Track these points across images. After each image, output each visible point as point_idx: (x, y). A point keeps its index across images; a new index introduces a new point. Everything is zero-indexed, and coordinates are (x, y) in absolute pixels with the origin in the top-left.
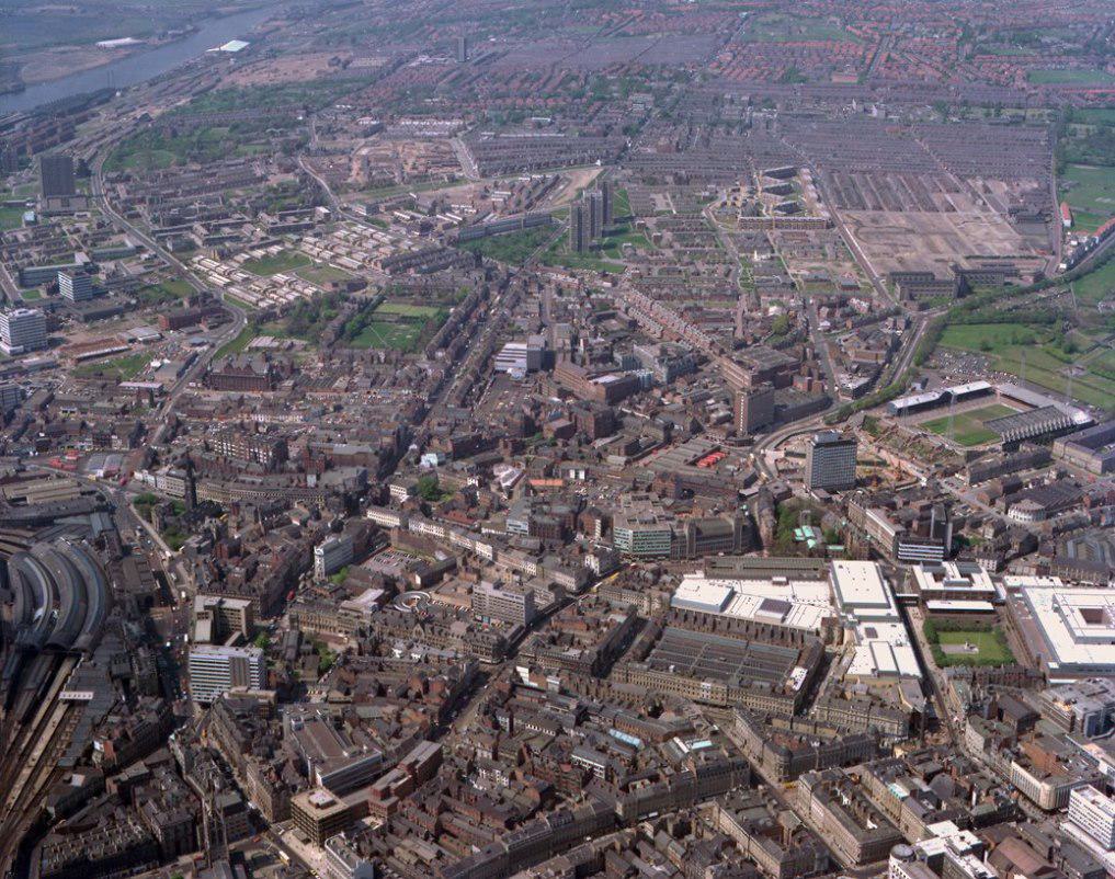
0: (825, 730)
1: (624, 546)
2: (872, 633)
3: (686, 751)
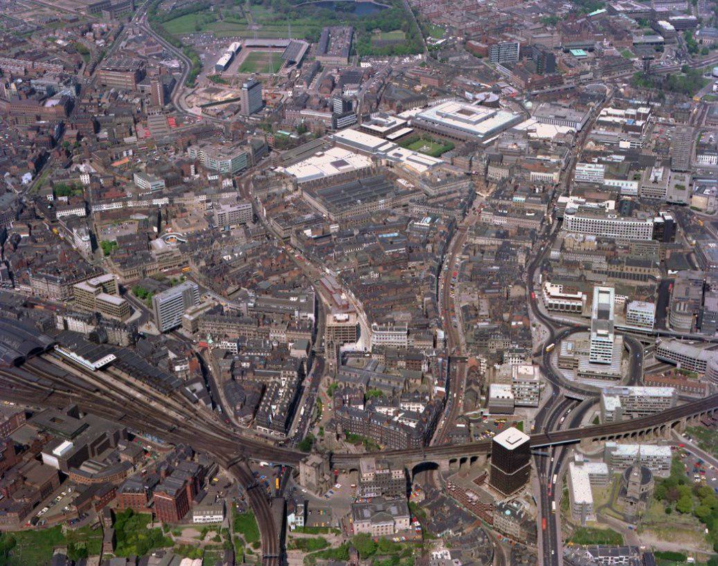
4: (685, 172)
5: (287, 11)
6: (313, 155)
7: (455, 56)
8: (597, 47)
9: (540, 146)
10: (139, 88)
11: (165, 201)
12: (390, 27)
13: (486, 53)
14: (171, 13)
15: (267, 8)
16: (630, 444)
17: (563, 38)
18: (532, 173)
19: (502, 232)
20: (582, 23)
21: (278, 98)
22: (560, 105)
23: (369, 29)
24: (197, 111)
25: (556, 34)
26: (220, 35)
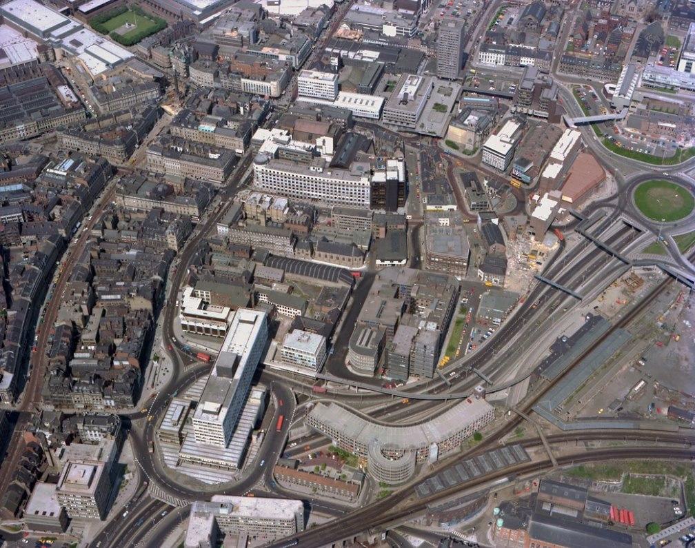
0: (121, 116)
2: (77, 43)
3: (65, 174)
4: (455, 80)
16: (486, 140)
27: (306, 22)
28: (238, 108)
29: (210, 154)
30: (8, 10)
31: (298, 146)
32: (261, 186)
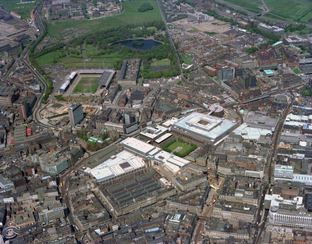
1: (54, 172)
3: (179, 222)
5: (105, 48)
6: (109, 158)
7: (198, 77)
8: (279, 68)
9: (250, 146)
10: (14, 106)
11: (10, 200)
12: (162, 57)
13: (215, 74)
14: (42, 51)
15: (95, 46)
17: (259, 62)
18: (246, 171)
19: (228, 227)
20: (270, 51)
21: (94, 111)
22: (261, 114)
23: (150, 59)
24: (45, 121)
25: (255, 61)
26: (66, 66)
27: (263, 142)
28: (249, 184)
29: (244, 208)
30: (126, 144)
31: (288, 202)
32: (273, 223)
